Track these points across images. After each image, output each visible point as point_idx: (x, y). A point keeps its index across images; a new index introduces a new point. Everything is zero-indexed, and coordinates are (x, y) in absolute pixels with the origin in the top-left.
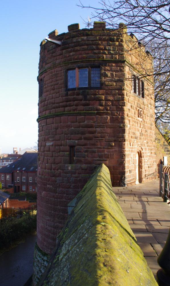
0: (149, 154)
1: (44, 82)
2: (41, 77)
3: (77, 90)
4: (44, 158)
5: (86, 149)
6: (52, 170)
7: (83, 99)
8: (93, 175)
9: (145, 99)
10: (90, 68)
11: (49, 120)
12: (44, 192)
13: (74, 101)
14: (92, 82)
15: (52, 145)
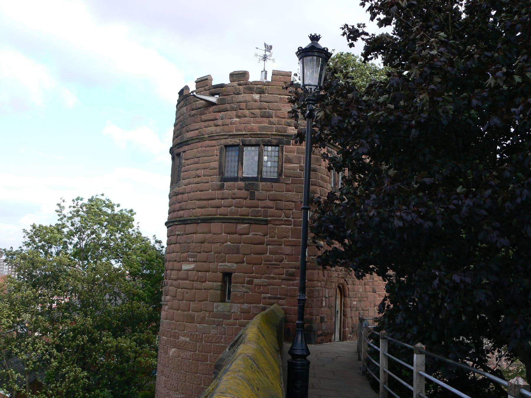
2: (177, 151)
7: (249, 196)
8: (486, 82)
12: (173, 350)
13: (234, 199)
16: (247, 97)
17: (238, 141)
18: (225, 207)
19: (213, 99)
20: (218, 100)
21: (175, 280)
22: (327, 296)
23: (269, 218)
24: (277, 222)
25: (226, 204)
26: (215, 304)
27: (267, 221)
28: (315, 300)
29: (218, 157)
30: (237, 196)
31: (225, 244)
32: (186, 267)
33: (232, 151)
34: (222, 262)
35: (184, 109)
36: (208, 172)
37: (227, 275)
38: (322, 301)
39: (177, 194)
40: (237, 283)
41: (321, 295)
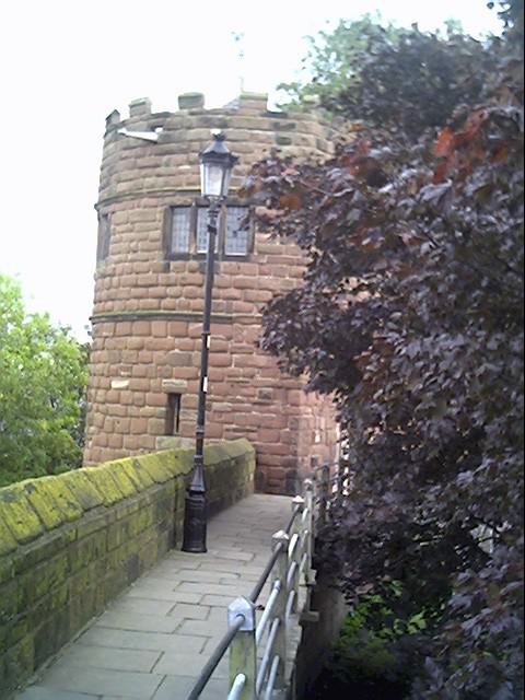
2: (104, 210)
13: (184, 285)
16: (202, 132)
17: (189, 200)
18: (172, 297)
19: (153, 136)
20: (161, 136)
21: (103, 403)
22: (323, 427)
23: (234, 315)
24: (246, 321)
25: (172, 293)
26: (158, 438)
27: (231, 318)
28: (301, 434)
29: (160, 224)
30: (188, 281)
31: (171, 352)
32: (116, 384)
33: (181, 214)
34: (166, 378)
35: (111, 146)
36: (147, 244)
37: (174, 397)
38: (314, 435)
39: (104, 276)
40: (188, 408)
41: (312, 425)
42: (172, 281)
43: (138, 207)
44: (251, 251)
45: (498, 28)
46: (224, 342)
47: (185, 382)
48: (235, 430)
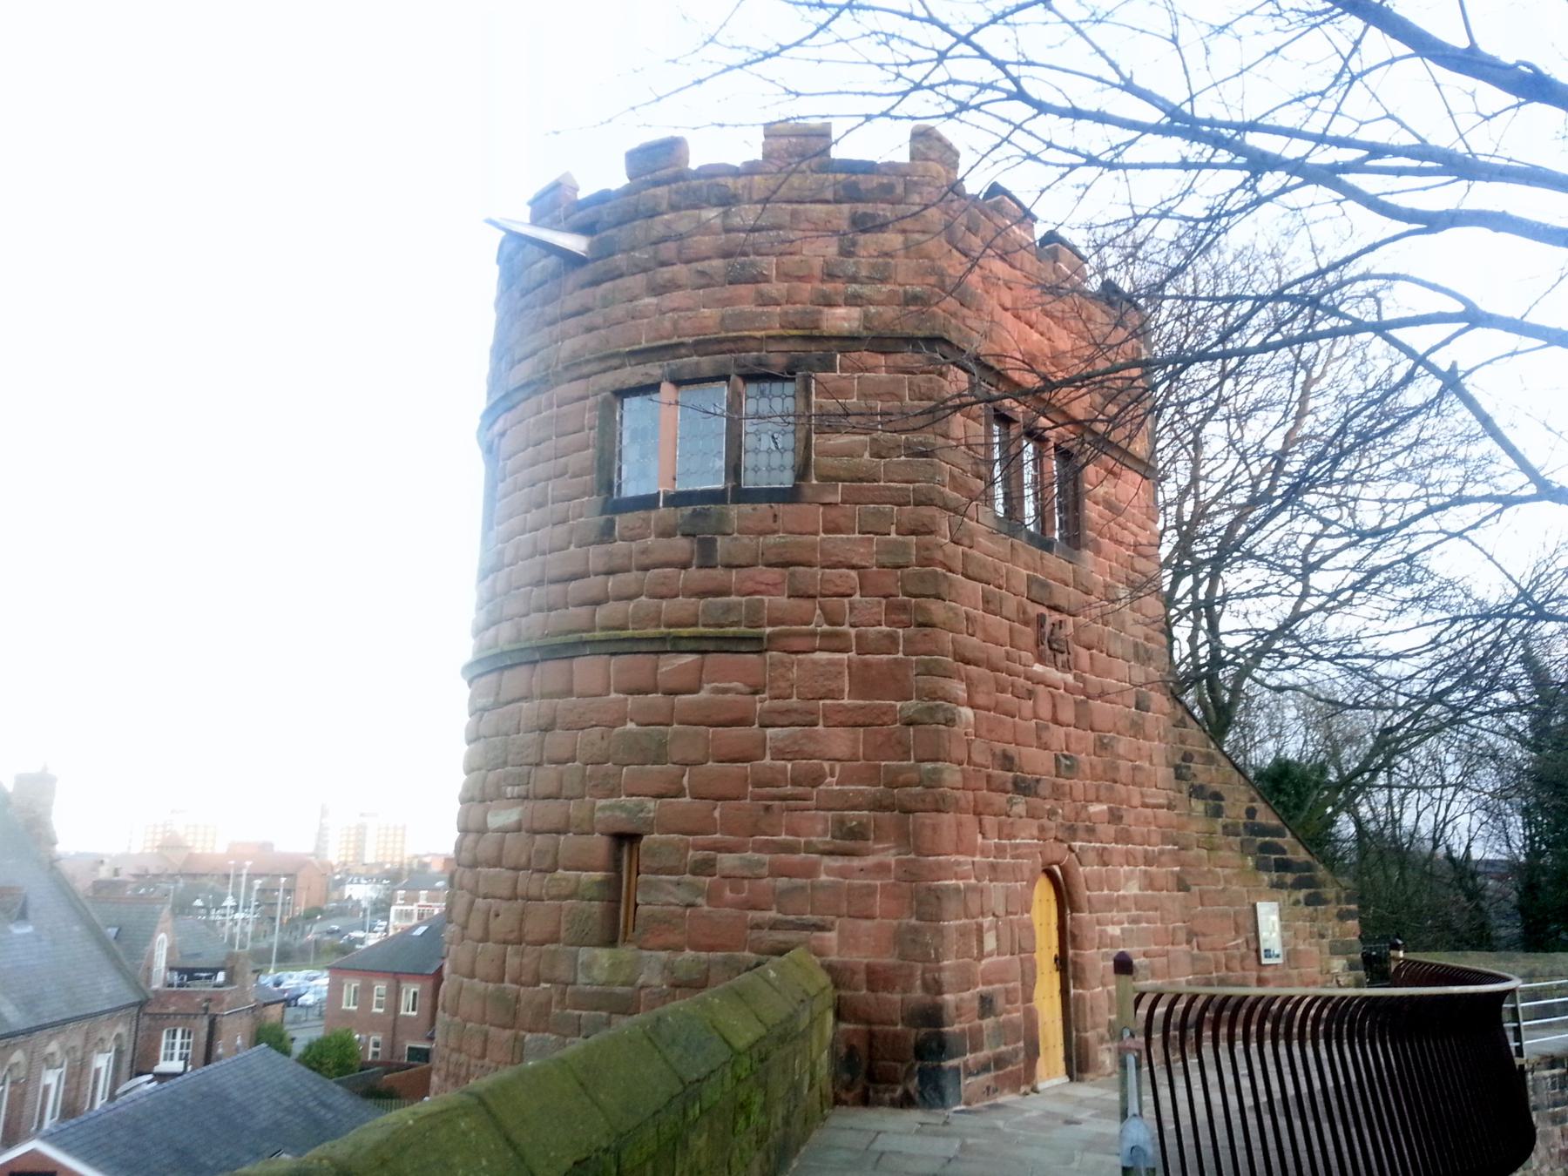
0: (1133, 889)
1: (501, 463)
3: (665, 506)
4: (472, 903)
5: (700, 854)
6: (502, 981)
9: (1088, 554)
10: (740, 383)
11: (587, 670)
13: (646, 569)
14: (747, 460)
15: (518, 828)
18: (619, 599)
24: (797, 644)
27: (759, 639)
30: (657, 557)
40: (656, 872)
42: (618, 562)
43: (550, 406)
44: (802, 472)
45: (832, 156)
46: (749, 697)
47: (651, 804)
48: (775, 926)
